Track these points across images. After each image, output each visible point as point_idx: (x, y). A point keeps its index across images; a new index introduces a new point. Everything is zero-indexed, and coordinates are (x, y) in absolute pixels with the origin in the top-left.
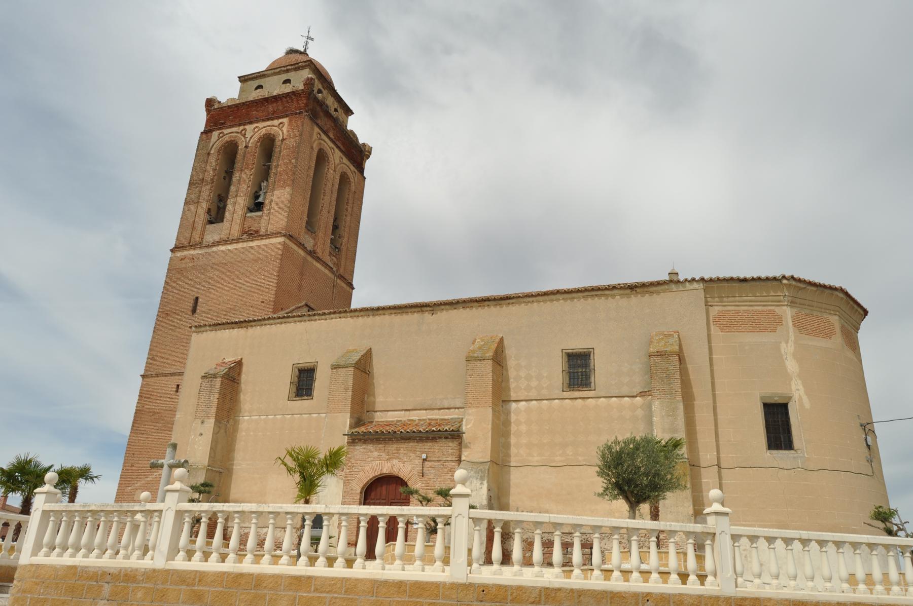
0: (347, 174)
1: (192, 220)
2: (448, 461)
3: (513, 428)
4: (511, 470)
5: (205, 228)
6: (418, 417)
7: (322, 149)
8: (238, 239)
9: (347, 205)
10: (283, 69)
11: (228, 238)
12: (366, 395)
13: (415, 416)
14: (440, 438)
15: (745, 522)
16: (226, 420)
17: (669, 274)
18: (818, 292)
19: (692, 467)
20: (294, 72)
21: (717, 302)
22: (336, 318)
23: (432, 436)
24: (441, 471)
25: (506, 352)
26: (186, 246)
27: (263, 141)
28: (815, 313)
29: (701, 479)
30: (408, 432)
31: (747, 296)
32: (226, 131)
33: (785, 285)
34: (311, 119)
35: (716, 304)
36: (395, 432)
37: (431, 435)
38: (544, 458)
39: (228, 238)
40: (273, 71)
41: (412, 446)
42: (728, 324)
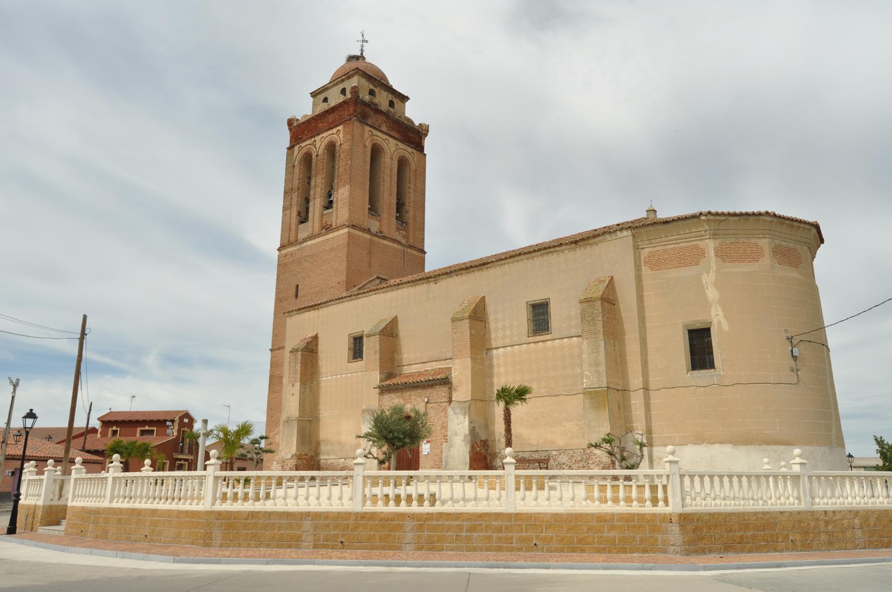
1: (288, 223)
3: (496, 370)
5: (298, 228)
6: (431, 367)
8: (319, 234)
11: (312, 234)
12: (396, 354)
13: (429, 367)
14: (436, 385)
15: (668, 434)
16: (310, 382)
17: (647, 211)
18: (741, 221)
19: (623, 392)
20: (347, 81)
22: (373, 295)
23: (431, 384)
26: (287, 245)
28: (741, 240)
30: (414, 382)
31: (672, 236)
32: (303, 145)
34: (360, 121)
36: (406, 383)
37: (431, 383)
39: (312, 234)
41: (419, 393)
42: (657, 263)
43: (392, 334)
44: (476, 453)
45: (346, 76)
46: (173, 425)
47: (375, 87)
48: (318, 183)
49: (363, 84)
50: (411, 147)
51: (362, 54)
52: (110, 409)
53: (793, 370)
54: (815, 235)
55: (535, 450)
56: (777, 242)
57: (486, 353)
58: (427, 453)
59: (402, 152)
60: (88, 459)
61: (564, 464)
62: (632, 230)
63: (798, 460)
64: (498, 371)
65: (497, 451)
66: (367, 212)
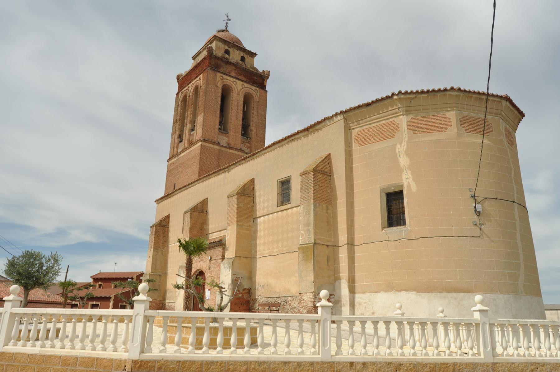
0: (250, 93)
3: (258, 234)
4: (257, 260)
7: (226, 84)
9: (253, 111)
12: (205, 225)
14: (216, 246)
15: (367, 282)
16: (162, 248)
19: (334, 247)
21: (356, 125)
27: (196, 90)
29: (339, 255)
31: (374, 116)
33: (396, 99)
35: (356, 127)
38: (270, 251)
40: (204, 47)
42: (364, 140)
43: (203, 211)
44: (238, 299)
45: (209, 42)
47: (230, 47)
48: (189, 113)
49: (220, 46)
50: (255, 86)
51: (226, 28)
52: (100, 271)
53: (476, 224)
54: (509, 107)
55: (278, 296)
56: (466, 113)
57: (253, 221)
58: (208, 299)
59: (247, 90)
60: (53, 301)
61: (295, 308)
62: (344, 114)
63: (479, 307)
64: (260, 234)
65: (257, 298)
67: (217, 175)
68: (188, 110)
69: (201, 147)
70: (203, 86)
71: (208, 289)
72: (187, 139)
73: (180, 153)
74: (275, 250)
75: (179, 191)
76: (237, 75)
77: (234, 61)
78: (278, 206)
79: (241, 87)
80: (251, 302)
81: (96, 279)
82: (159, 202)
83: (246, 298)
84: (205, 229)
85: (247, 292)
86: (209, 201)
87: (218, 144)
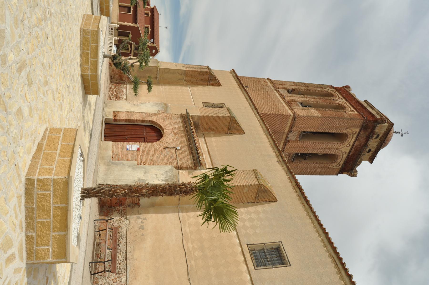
0: (337, 160)
2: (177, 160)
4: (176, 214)
6: (206, 158)
7: (347, 137)
10: (381, 115)
12: (214, 132)
14: (193, 157)
16: (186, 79)
22: (258, 119)
24: (169, 157)
25: (266, 205)
27: (340, 106)
32: (337, 93)
34: (363, 125)
38: (189, 235)
40: (377, 111)
46: (151, 43)
48: (318, 100)
49: (383, 129)
52: (160, 14)
59: (340, 157)
65: (127, 217)
66: (303, 130)
67: (272, 146)
68: (320, 99)
69: (288, 115)
70: (346, 114)
71: (139, 147)
72: (293, 98)
73: (278, 92)
74: (190, 245)
75: (247, 97)
76: (355, 147)
77: (369, 144)
78: (249, 246)
79: (343, 151)
80: (121, 208)
81: (153, 10)
82: (233, 73)
83: (127, 201)
84: (210, 132)
85: (134, 202)
86: (242, 135)
87: (290, 131)
